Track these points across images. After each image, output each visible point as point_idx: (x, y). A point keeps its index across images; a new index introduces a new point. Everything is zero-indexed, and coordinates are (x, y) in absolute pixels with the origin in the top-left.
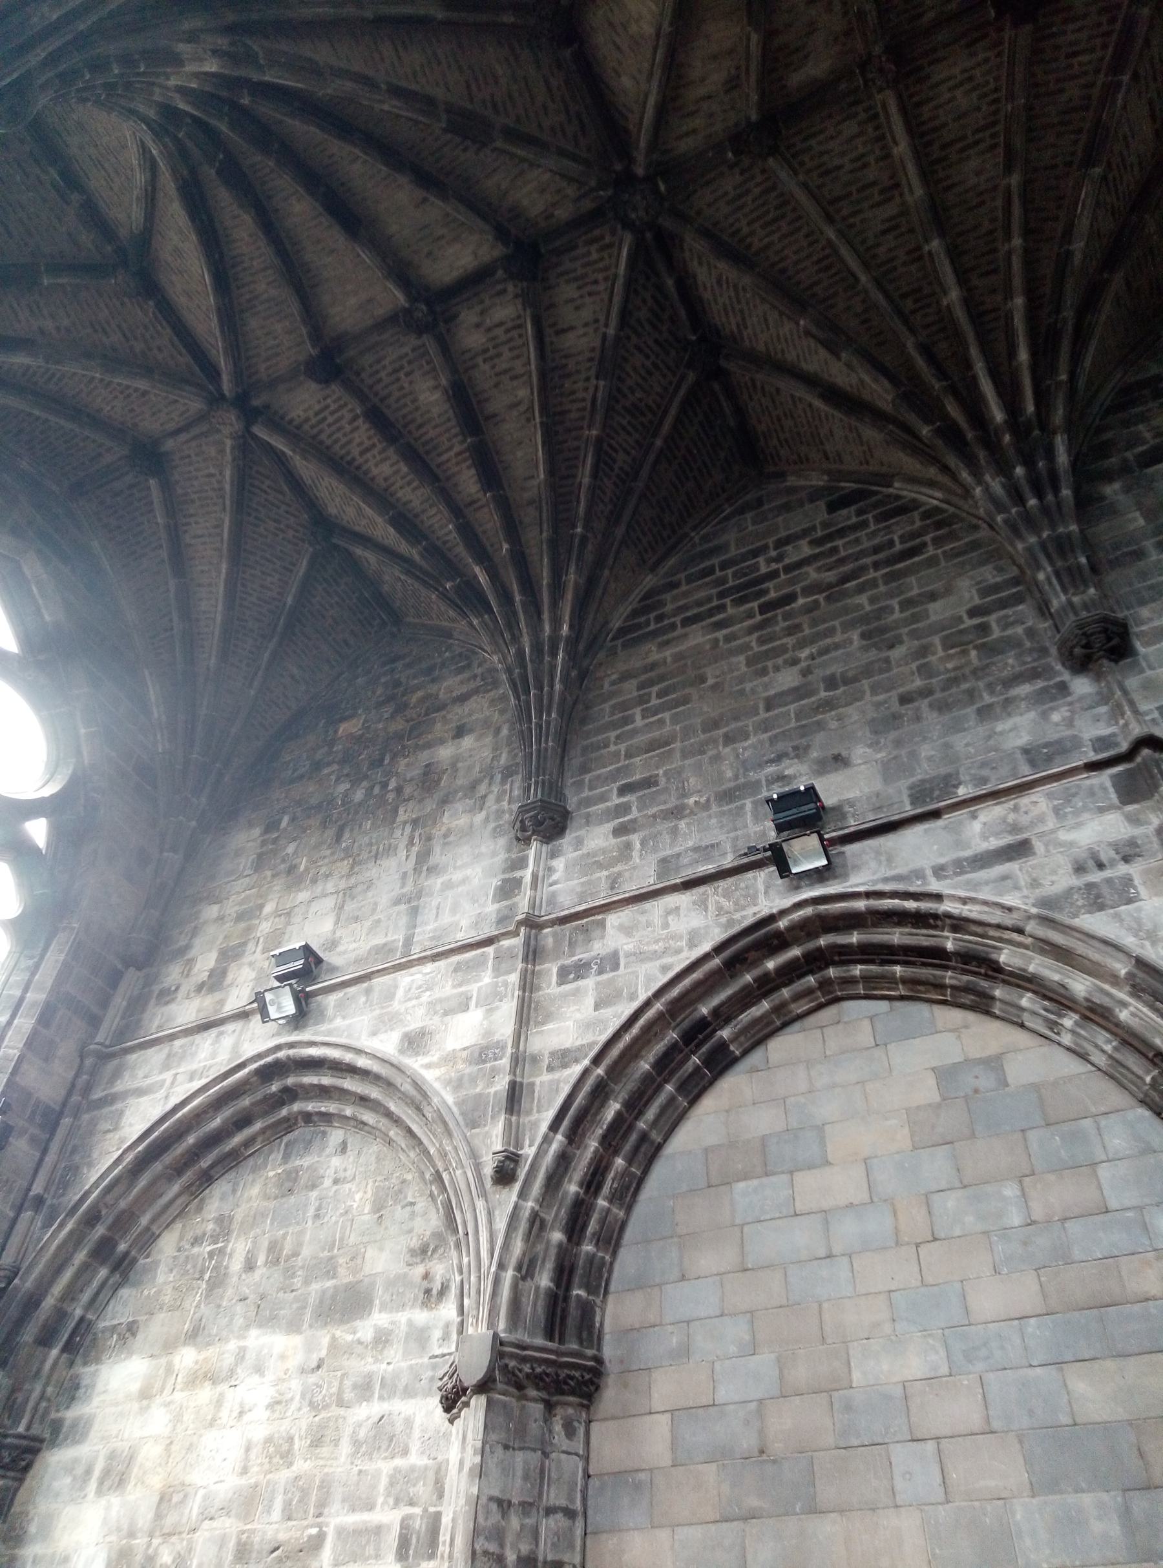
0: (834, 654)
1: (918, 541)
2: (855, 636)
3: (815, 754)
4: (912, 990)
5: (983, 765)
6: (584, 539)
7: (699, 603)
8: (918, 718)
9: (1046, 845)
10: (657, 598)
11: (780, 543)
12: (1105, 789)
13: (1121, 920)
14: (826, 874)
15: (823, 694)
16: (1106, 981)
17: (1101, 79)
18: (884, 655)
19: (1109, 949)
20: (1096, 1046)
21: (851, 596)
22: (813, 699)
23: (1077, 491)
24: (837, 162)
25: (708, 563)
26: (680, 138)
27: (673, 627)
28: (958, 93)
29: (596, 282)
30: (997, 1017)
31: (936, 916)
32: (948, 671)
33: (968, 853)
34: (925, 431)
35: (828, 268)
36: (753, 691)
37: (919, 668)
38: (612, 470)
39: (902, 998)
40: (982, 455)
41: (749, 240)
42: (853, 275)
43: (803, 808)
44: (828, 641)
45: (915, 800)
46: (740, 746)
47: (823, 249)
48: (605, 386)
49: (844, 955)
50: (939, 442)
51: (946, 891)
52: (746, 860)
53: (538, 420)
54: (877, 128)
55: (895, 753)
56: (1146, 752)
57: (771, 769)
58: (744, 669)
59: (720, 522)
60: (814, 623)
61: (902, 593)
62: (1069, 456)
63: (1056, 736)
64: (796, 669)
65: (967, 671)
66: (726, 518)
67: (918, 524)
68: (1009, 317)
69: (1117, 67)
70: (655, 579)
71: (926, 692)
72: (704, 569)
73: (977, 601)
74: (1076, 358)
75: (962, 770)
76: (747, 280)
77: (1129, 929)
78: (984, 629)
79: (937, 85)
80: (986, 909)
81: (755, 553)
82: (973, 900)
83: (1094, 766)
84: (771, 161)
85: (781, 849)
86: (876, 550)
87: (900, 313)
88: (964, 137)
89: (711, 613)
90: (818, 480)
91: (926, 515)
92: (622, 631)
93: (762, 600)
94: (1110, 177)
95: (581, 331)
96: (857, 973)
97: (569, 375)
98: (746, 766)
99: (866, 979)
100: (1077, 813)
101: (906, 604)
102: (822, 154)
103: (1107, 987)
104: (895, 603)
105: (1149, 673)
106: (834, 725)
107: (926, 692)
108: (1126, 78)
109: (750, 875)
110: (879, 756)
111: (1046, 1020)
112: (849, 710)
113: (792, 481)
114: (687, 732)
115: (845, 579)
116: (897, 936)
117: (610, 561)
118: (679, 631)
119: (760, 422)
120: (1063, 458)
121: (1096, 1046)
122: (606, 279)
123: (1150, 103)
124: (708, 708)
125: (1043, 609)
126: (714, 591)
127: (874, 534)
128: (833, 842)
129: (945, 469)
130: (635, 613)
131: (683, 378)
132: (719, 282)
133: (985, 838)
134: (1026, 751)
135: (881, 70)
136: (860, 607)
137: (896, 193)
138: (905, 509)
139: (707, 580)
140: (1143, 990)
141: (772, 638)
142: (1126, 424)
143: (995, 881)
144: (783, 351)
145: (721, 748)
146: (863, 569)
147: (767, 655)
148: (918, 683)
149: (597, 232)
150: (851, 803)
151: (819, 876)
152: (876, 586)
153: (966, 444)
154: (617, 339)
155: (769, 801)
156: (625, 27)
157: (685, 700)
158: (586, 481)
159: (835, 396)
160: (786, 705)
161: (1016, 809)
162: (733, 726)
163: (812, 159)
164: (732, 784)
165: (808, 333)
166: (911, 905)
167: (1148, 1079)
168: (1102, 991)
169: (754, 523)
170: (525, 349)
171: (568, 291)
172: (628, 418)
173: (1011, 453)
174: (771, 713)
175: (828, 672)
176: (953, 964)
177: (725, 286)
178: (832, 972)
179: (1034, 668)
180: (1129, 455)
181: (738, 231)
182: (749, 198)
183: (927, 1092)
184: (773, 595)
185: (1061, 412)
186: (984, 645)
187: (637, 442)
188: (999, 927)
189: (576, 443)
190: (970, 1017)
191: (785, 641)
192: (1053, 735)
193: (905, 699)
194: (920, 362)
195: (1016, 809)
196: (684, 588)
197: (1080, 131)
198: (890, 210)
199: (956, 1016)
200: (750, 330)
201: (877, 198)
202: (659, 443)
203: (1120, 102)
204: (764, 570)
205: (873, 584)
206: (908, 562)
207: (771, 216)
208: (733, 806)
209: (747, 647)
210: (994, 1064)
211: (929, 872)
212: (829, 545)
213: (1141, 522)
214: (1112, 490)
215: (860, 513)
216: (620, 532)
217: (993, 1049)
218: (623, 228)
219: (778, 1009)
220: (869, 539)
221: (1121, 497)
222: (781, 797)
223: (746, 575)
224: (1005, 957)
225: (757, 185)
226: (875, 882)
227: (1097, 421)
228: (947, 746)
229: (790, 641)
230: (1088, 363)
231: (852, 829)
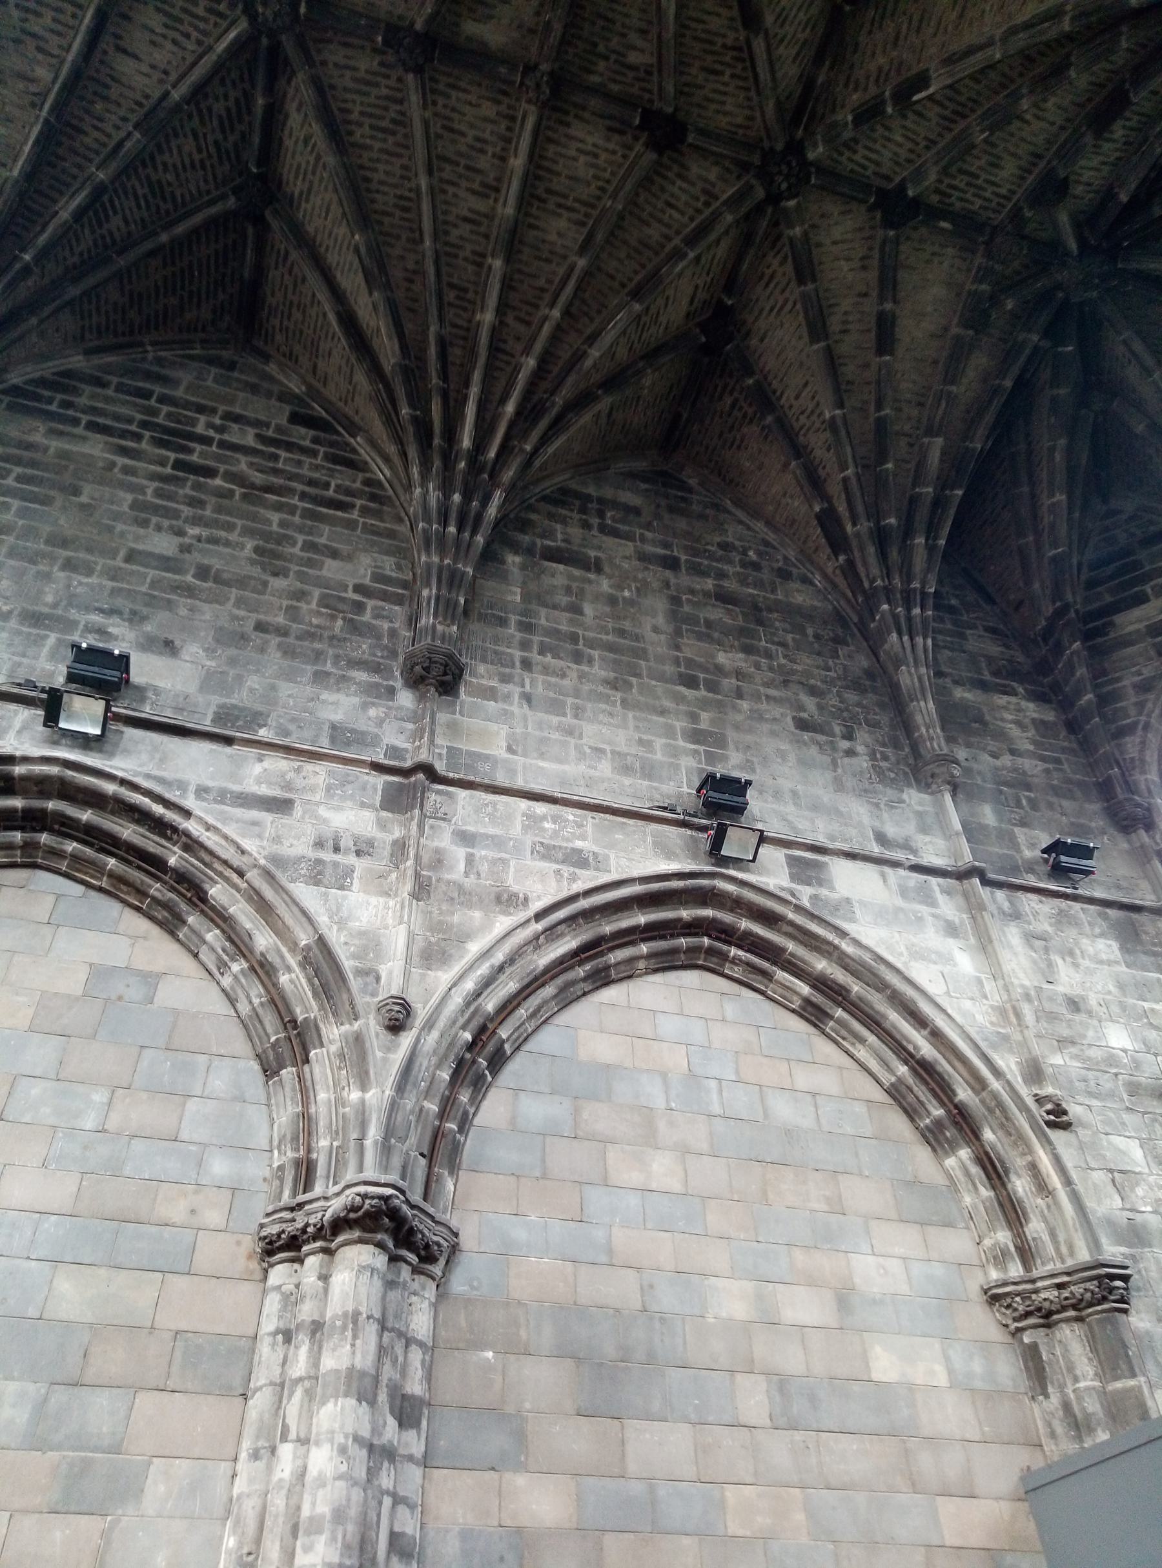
0: (221, 549)
1: (348, 499)
2: (250, 545)
3: (149, 628)
4: (114, 886)
5: (293, 720)
6: (26, 270)
7: (117, 417)
8: (262, 650)
9: (304, 813)
10: (73, 383)
11: (228, 416)
12: (376, 790)
13: (326, 901)
14: (93, 744)
15: (189, 578)
16: (286, 945)
17: (677, 241)
18: (265, 577)
19: (304, 919)
20: (248, 997)
21: (266, 507)
22: (177, 577)
23: (488, 544)
24: (463, 127)
25: (148, 386)
27: (76, 422)
28: (582, 159)
29: (187, 36)
30: (178, 940)
31: (175, 830)
32: (311, 624)
33: (236, 788)
34: (405, 411)
35: (406, 209)
36: (122, 535)
37: (289, 608)
38: (100, 226)
39: (101, 890)
40: (437, 463)
41: (353, 127)
42: (421, 234)
43: (106, 671)
44: (223, 534)
45: (218, 718)
46: (77, 578)
47: (410, 190)
48: (139, 141)
49: (65, 827)
50: (411, 429)
51: (197, 812)
52: (16, 690)
53: (44, 113)
54: (509, 129)
55: (225, 668)
56: (421, 776)
57: (96, 618)
58: (125, 508)
59: (183, 356)
60: (219, 509)
61: (311, 534)
62: (499, 511)
63: (364, 728)
64: (177, 540)
65: (326, 634)
66: (191, 358)
67: (358, 485)
68: (517, 369)
69: (692, 240)
70: (84, 364)
71: (282, 632)
72: (140, 389)
73: (367, 581)
74: (544, 440)
75: (274, 715)
76: (331, 160)
77: (329, 910)
78: (359, 607)
79: (571, 138)
80: (223, 843)
81: (201, 409)
82: (216, 830)
83: (377, 767)
84: (410, 77)
85: (61, 697)
86: (311, 483)
87: (440, 297)
88: (565, 197)
89: (123, 434)
90: (295, 386)
91: (368, 482)
92: (15, 391)
93: (182, 456)
94: (644, 319)
95: (145, 69)
96: (70, 849)
97: (106, 99)
98: (72, 600)
99: (75, 858)
100: (343, 798)
101: (310, 546)
102: (453, 110)
103: (284, 950)
104: (300, 539)
105: (458, 716)
106: (183, 612)
107: (282, 632)
108: (691, 255)
109: (13, 707)
110: (208, 663)
111: (219, 959)
112: (205, 607)
113: (272, 368)
114: (28, 533)
115: (268, 489)
116: (128, 832)
117: (47, 311)
118: (79, 430)
119: (273, 295)
120: (492, 511)
121: (248, 997)
123: (697, 287)
124: (65, 523)
125: (413, 620)
126: (139, 416)
127: (317, 468)
128: (118, 718)
129: (404, 454)
130: (42, 382)
131: (223, 197)
132: (306, 141)
133: (259, 783)
134: (334, 727)
135: (538, 86)
136: (269, 522)
137: (493, 195)
138: (354, 465)
139: (138, 400)
140: (310, 964)
141: (170, 497)
142: (551, 516)
143: (245, 822)
144: (327, 250)
145: (55, 569)
146: (291, 491)
147: (156, 510)
148: (280, 620)
150: (157, 691)
151: (85, 742)
152: (293, 514)
153: (430, 445)
154: (177, 109)
155: (76, 647)
157: (46, 501)
158: (65, 215)
159: (349, 321)
160: (146, 566)
161: (298, 770)
162: (82, 555)
163: (445, 106)
164: (46, 610)
165: (357, 250)
166: (158, 809)
167: (273, 1039)
168: (279, 951)
169: (215, 381)
170: (71, 33)
172: (146, 190)
173: (459, 478)
174: (128, 566)
175: (206, 562)
176: (167, 878)
178: (44, 838)
179: (379, 664)
180: (539, 542)
182: (374, 91)
183: (73, 983)
184: (194, 458)
185: (511, 473)
186: (351, 620)
187: (143, 220)
188: (225, 862)
189: (75, 171)
190: (155, 931)
191: (182, 507)
192: (362, 726)
193: (260, 627)
194: (433, 351)
195: (298, 770)
196: (110, 392)
197: (643, 266)
198: (481, 206)
199: (142, 925)
200: (309, 206)
201: (476, 186)
202: (164, 238)
203: (678, 269)
204: (200, 429)
205: (292, 510)
206: (332, 512)
208: (34, 631)
209: (142, 490)
210: (151, 980)
211: (192, 788)
212: (273, 450)
213: (518, 598)
214: (513, 560)
215: (315, 440)
216: (74, 291)
217: (158, 966)
218: (244, 12)
220: (310, 469)
221: (516, 570)
222: (91, 650)
223: (179, 422)
224: (217, 892)
225: (387, 87)
226: (137, 774)
227: (532, 501)
228: (273, 688)
229: (186, 511)
230: (551, 450)
231: (143, 715)
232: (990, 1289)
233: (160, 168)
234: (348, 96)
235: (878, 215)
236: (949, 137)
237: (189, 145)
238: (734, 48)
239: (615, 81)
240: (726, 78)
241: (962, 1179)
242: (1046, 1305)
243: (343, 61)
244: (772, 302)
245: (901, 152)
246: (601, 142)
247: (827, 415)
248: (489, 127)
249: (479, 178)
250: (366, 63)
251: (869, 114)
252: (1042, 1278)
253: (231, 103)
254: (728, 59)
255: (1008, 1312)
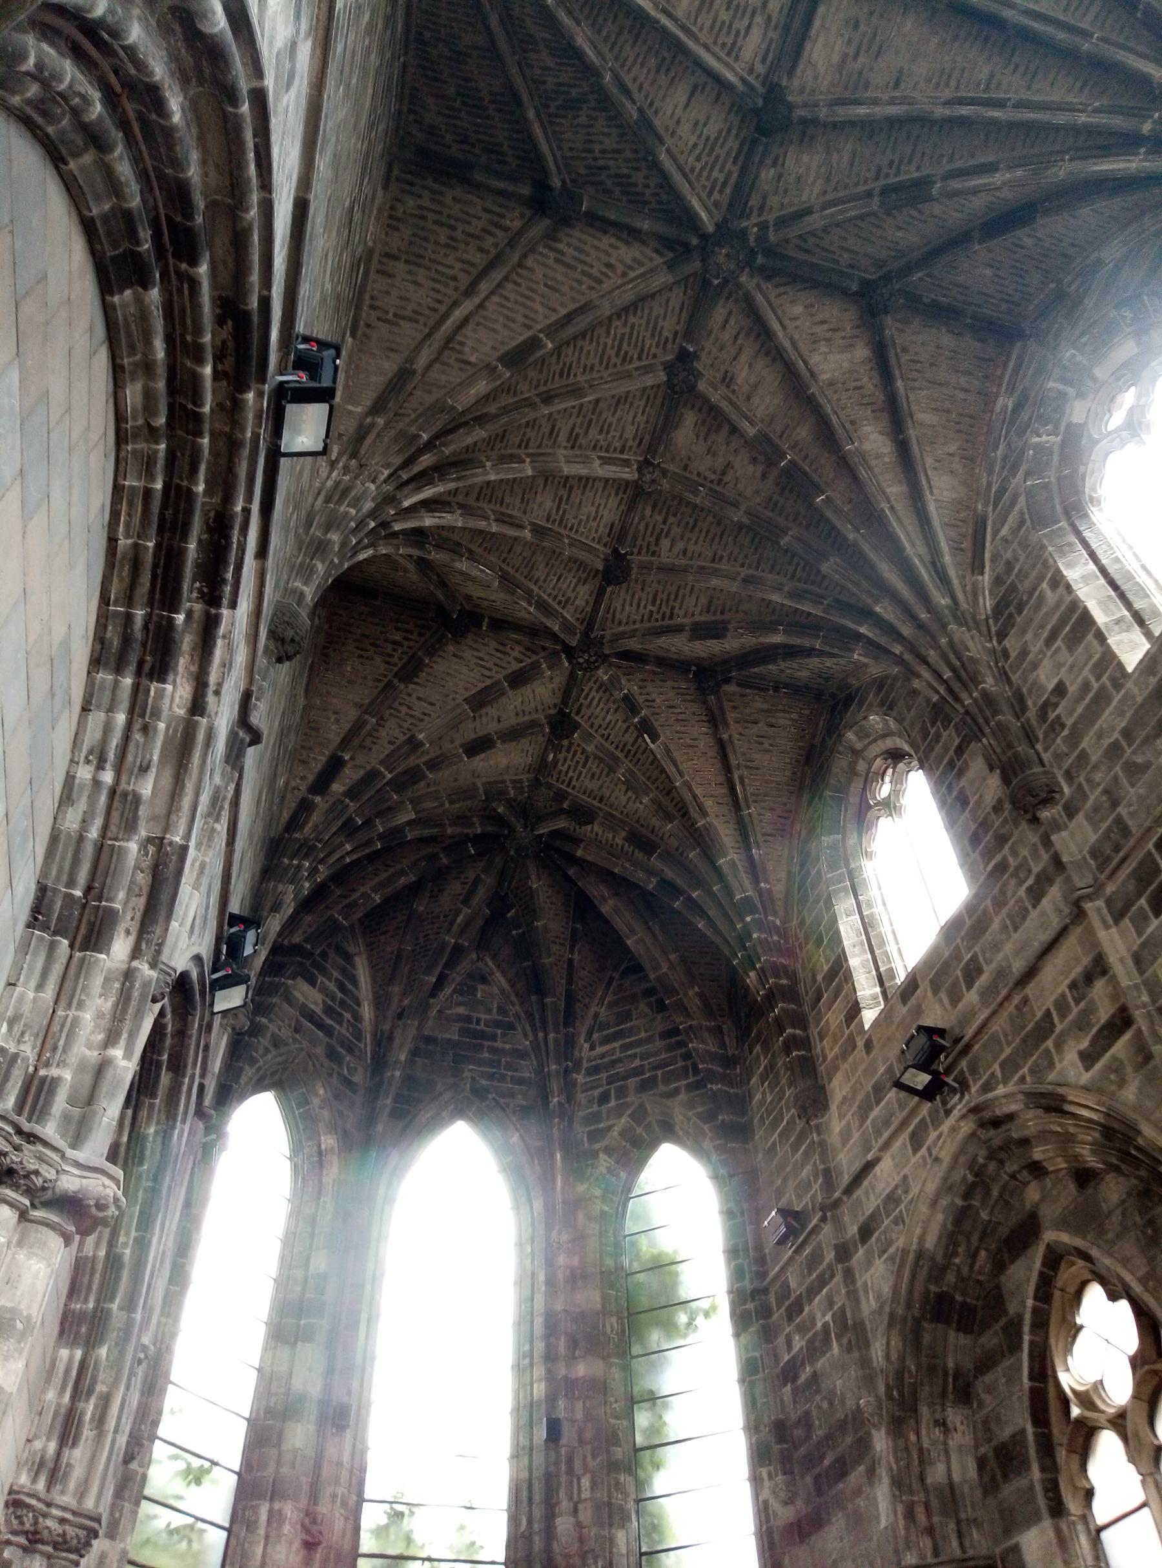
4: (124, 558)
24: (618, 413)
26: (730, 313)
28: (593, 509)
29: (698, 159)
39: (112, 540)
95: (679, 113)
102: (631, 404)
122: (693, 170)
132: (609, 266)
149: (728, 190)
156: (828, 340)
171: (713, 128)
177: (604, 270)
181: (635, 314)
182: (648, 335)
187: (544, 83)
200: (551, 262)
201: (577, 430)
202: (531, 114)
207: (625, 344)
219: (148, 367)
232: (18, 1493)
233: (594, 114)
234: (646, 311)
235: (553, 711)
236: (612, 748)
237: (610, 143)
238: (672, 613)
239: (647, 525)
240: (650, 607)
241: (61, 1374)
242: (45, 1533)
243: (671, 304)
244: (486, 657)
245: (599, 720)
246: (603, 521)
247: (421, 736)
248: (618, 435)
249: (582, 432)
250: (668, 326)
251: (630, 705)
252: (58, 1507)
253: (640, 189)
254: (664, 609)
255: (15, 1522)
